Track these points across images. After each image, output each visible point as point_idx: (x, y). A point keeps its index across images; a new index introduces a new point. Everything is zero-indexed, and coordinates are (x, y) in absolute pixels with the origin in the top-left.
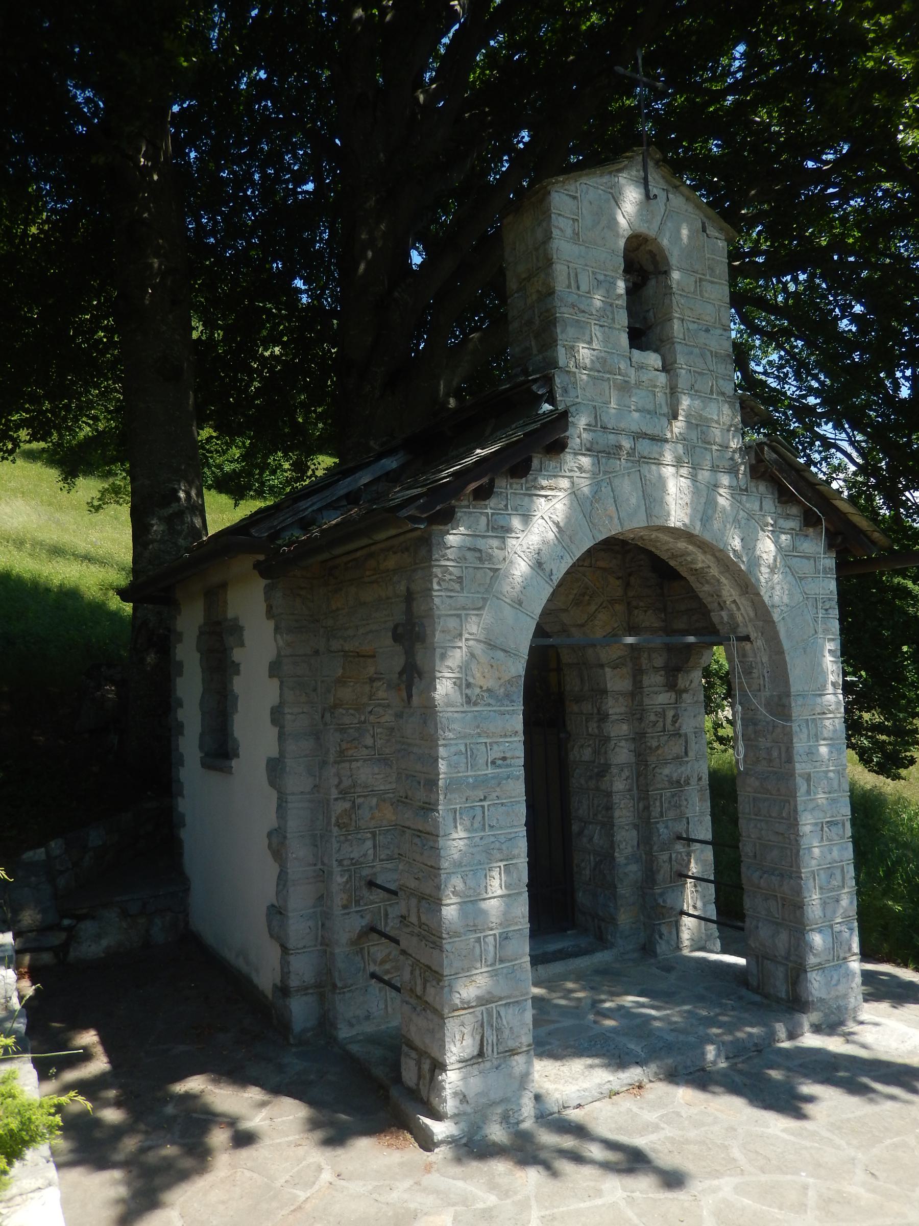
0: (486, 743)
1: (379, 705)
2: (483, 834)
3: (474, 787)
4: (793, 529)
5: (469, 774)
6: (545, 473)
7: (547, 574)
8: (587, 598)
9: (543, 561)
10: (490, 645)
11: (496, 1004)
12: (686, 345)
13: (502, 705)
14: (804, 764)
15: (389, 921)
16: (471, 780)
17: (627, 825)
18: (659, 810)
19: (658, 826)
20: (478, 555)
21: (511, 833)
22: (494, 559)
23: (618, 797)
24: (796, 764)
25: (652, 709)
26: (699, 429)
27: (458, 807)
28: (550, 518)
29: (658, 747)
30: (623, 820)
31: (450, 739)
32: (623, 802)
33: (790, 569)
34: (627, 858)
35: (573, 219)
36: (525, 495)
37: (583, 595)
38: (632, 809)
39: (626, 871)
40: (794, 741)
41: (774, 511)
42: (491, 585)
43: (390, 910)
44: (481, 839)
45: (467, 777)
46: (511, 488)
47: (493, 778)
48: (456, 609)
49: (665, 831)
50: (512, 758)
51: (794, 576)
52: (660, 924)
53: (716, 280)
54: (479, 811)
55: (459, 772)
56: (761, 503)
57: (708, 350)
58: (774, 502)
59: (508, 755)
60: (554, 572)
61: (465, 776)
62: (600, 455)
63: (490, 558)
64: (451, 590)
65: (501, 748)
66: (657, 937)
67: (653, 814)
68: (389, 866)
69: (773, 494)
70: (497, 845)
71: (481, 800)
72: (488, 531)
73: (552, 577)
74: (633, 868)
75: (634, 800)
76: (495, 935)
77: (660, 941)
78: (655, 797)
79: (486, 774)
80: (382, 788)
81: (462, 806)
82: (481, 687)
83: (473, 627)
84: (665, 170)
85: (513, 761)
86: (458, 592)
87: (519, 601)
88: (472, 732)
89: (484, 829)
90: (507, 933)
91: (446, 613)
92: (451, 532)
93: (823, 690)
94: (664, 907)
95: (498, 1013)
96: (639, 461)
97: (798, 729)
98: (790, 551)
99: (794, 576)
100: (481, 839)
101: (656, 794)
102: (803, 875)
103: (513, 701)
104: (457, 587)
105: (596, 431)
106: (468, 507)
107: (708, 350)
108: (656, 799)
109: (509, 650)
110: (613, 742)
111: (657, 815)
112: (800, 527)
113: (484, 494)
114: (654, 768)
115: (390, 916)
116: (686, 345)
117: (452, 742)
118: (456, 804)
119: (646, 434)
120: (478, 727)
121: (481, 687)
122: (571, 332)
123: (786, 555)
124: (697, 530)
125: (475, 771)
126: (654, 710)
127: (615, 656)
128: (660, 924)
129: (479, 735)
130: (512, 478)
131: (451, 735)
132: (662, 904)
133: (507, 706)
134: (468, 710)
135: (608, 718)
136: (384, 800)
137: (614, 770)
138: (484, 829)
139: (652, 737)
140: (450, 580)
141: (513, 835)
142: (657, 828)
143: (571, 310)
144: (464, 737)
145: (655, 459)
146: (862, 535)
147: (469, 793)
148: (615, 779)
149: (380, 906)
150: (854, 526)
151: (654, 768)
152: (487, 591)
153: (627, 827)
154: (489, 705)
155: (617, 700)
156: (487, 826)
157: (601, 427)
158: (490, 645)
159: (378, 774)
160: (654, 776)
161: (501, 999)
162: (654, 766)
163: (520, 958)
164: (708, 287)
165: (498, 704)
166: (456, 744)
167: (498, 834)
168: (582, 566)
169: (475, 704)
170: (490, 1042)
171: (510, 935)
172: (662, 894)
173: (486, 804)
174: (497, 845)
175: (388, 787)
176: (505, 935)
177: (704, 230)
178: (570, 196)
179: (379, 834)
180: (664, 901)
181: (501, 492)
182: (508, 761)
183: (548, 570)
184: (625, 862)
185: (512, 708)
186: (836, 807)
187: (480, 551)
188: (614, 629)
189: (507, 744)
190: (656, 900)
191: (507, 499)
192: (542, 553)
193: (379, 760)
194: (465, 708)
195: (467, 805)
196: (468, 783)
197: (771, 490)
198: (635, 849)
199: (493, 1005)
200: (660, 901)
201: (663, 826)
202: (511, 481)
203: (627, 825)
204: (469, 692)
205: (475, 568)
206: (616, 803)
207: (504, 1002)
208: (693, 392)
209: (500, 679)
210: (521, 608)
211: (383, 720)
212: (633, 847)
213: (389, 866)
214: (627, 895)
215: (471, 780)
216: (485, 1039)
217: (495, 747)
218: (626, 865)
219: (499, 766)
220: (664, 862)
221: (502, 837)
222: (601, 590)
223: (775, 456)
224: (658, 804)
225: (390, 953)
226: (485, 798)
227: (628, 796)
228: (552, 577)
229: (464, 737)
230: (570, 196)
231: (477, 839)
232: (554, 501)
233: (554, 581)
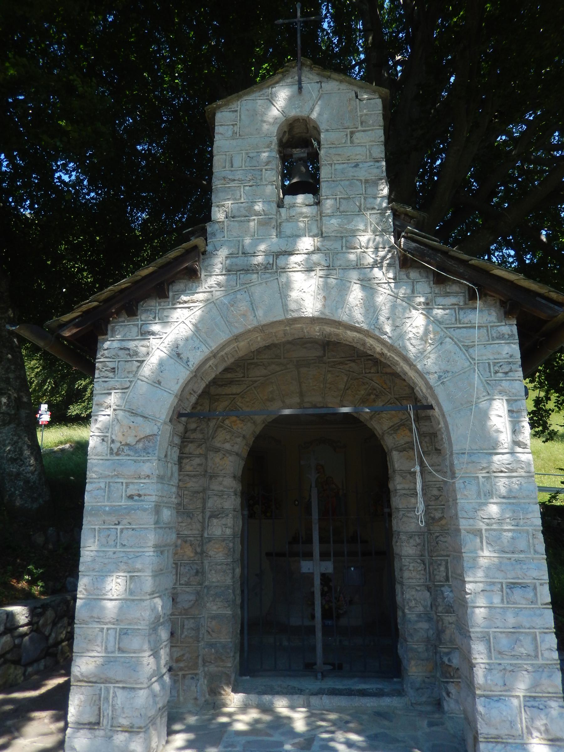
0: (122, 483)
1: (188, 475)
2: (115, 550)
3: (109, 514)
4: (455, 304)
5: (106, 504)
6: (189, 292)
7: (185, 362)
8: (373, 397)
9: (180, 352)
10: (132, 413)
11: (114, 685)
12: (333, 181)
13: (140, 456)
14: (471, 520)
15: (185, 630)
16: (107, 509)
17: (419, 586)
18: (445, 574)
19: (443, 589)
20: (127, 352)
21: (138, 552)
22: (140, 354)
23: (408, 560)
24: (460, 520)
25: (435, 485)
26: (344, 240)
27: (97, 527)
28: (190, 322)
29: (441, 518)
30: (414, 581)
31: (95, 478)
32: (412, 565)
33: (453, 340)
34: (419, 616)
35: (233, 125)
36: (171, 308)
37: (369, 394)
38: (423, 572)
39: (416, 627)
40: (458, 497)
41: (429, 291)
42: (137, 372)
43: (186, 622)
44: (114, 553)
45: (105, 506)
46: (160, 306)
47: (125, 508)
48: (108, 390)
49: (451, 594)
50: (145, 495)
51: (458, 346)
52: (447, 682)
53: (367, 128)
54: (113, 532)
55: (98, 502)
56: (413, 287)
57: (357, 180)
58: (429, 284)
59: (141, 493)
60: (191, 359)
61: (103, 505)
62: (238, 273)
63: (136, 354)
64: (107, 377)
65: (136, 487)
66: (444, 694)
67: (437, 577)
68: (187, 590)
69: (427, 277)
70: (125, 559)
71: (115, 524)
72: (137, 336)
73: (188, 363)
74: (424, 625)
75: (424, 564)
76: (116, 629)
77: (447, 698)
78: (439, 562)
79: (120, 506)
80: (186, 532)
81: (101, 527)
82: (121, 443)
83: (113, 399)
84: (317, 69)
85: (146, 497)
86: (112, 378)
87: (158, 381)
88: (110, 474)
89: (116, 546)
90: (128, 629)
91: (101, 392)
92: (109, 339)
93: (495, 449)
94: (450, 666)
95: (114, 693)
96: (276, 272)
97: (462, 486)
98: (453, 324)
99: (458, 346)
100: (114, 553)
101: (441, 560)
102: (472, 635)
103: (148, 453)
104: (111, 375)
105: (238, 257)
106: (124, 322)
107: (357, 180)
108: (440, 565)
109: (147, 416)
110: (401, 513)
111: (442, 579)
112: (465, 301)
113: (132, 312)
114: (437, 537)
115: (186, 627)
116: (333, 181)
117: (95, 480)
118: (95, 525)
119: (286, 252)
120: (115, 470)
121: (121, 443)
122: (221, 195)
123: (446, 328)
124: (328, 314)
125: (111, 502)
126: (438, 486)
127: (402, 442)
128: (447, 682)
129: (117, 476)
130: (160, 298)
131: (94, 476)
132: (447, 662)
133: (144, 456)
134: (110, 458)
135: (397, 493)
136: (186, 542)
137: (403, 537)
138: (116, 546)
139: (436, 510)
140: (106, 370)
141: (140, 554)
142: (442, 591)
143: (222, 182)
144: (106, 477)
145: (293, 268)
146: (538, 299)
147: (106, 518)
148: (404, 544)
149: (178, 618)
150: (527, 291)
151: (437, 537)
152: (134, 376)
153: (418, 588)
154: (129, 455)
155: (404, 478)
156: (118, 544)
157: (243, 253)
158: (132, 413)
159: (182, 522)
160: (437, 543)
161: (117, 682)
162: (438, 534)
163: (139, 653)
164: (359, 137)
165: (137, 455)
166: (99, 482)
167: (128, 552)
168: (370, 373)
169: (117, 454)
170: (106, 714)
171: (129, 631)
172: (448, 654)
173: (119, 527)
174: (125, 559)
175: (190, 532)
176: (125, 631)
177: (357, 97)
178: (233, 111)
179: (181, 566)
180: (449, 660)
181: (151, 309)
182: (142, 498)
183: (185, 358)
184: (416, 619)
185: (147, 458)
186: (521, 569)
187: (129, 349)
188: (402, 420)
189: (142, 485)
190: (441, 658)
191: (156, 314)
192: (180, 347)
193: (184, 513)
194: (109, 457)
195: (104, 527)
196: (105, 511)
197: (424, 275)
198: (428, 609)
199: (112, 685)
200: (446, 660)
201: (449, 590)
202: (159, 301)
203: (419, 586)
204: (112, 445)
205: (126, 361)
206: (405, 566)
207: (121, 685)
208: (338, 213)
209: (136, 436)
210: (159, 387)
211: (189, 485)
212: (425, 607)
213: (187, 590)
214: (420, 650)
215: (107, 509)
216: (101, 711)
217: (131, 486)
218: (417, 622)
219: (136, 501)
220: (450, 623)
221: (132, 554)
222: (388, 390)
223: (414, 245)
224: (442, 568)
225: (183, 655)
226: (119, 523)
227: (419, 561)
228: (188, 363)
229: (106, 477)
230: (233, 111)
231: (111, 553)
232: (195, 310)
233: (190, 366)
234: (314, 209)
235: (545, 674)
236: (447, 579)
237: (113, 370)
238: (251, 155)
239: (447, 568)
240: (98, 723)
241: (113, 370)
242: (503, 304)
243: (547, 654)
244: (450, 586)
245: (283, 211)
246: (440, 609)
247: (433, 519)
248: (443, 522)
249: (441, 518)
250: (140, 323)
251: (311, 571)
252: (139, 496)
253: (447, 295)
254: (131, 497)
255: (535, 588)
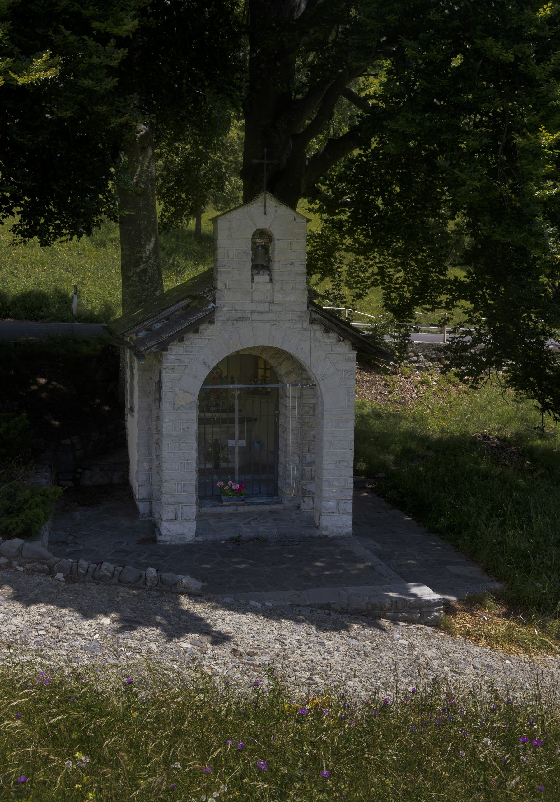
29: (309, 422)
66: (302, 502)
104: (171, 372)
169: (177, 410)
200: (304, 487)
224: (307, 446)
234: (269, 286)
235: (447, 372)
236: (309, 451)
237: (172, 369)
238: (238, 251)
239: (309, 446)
240: (176, 519)
241: (172, 369)
242: (353, 344)
243: (349, 485)
244: (309, 454)
245: (254, 285)
246: (304, 465)
247: (305, 422)
248: (310, 424)
249: (309, 422)
250: (184, 346)
251: (234, 445)
252: (188, 428)
253: (329, 338)
254: (184, 429)
255: (348, 462)
